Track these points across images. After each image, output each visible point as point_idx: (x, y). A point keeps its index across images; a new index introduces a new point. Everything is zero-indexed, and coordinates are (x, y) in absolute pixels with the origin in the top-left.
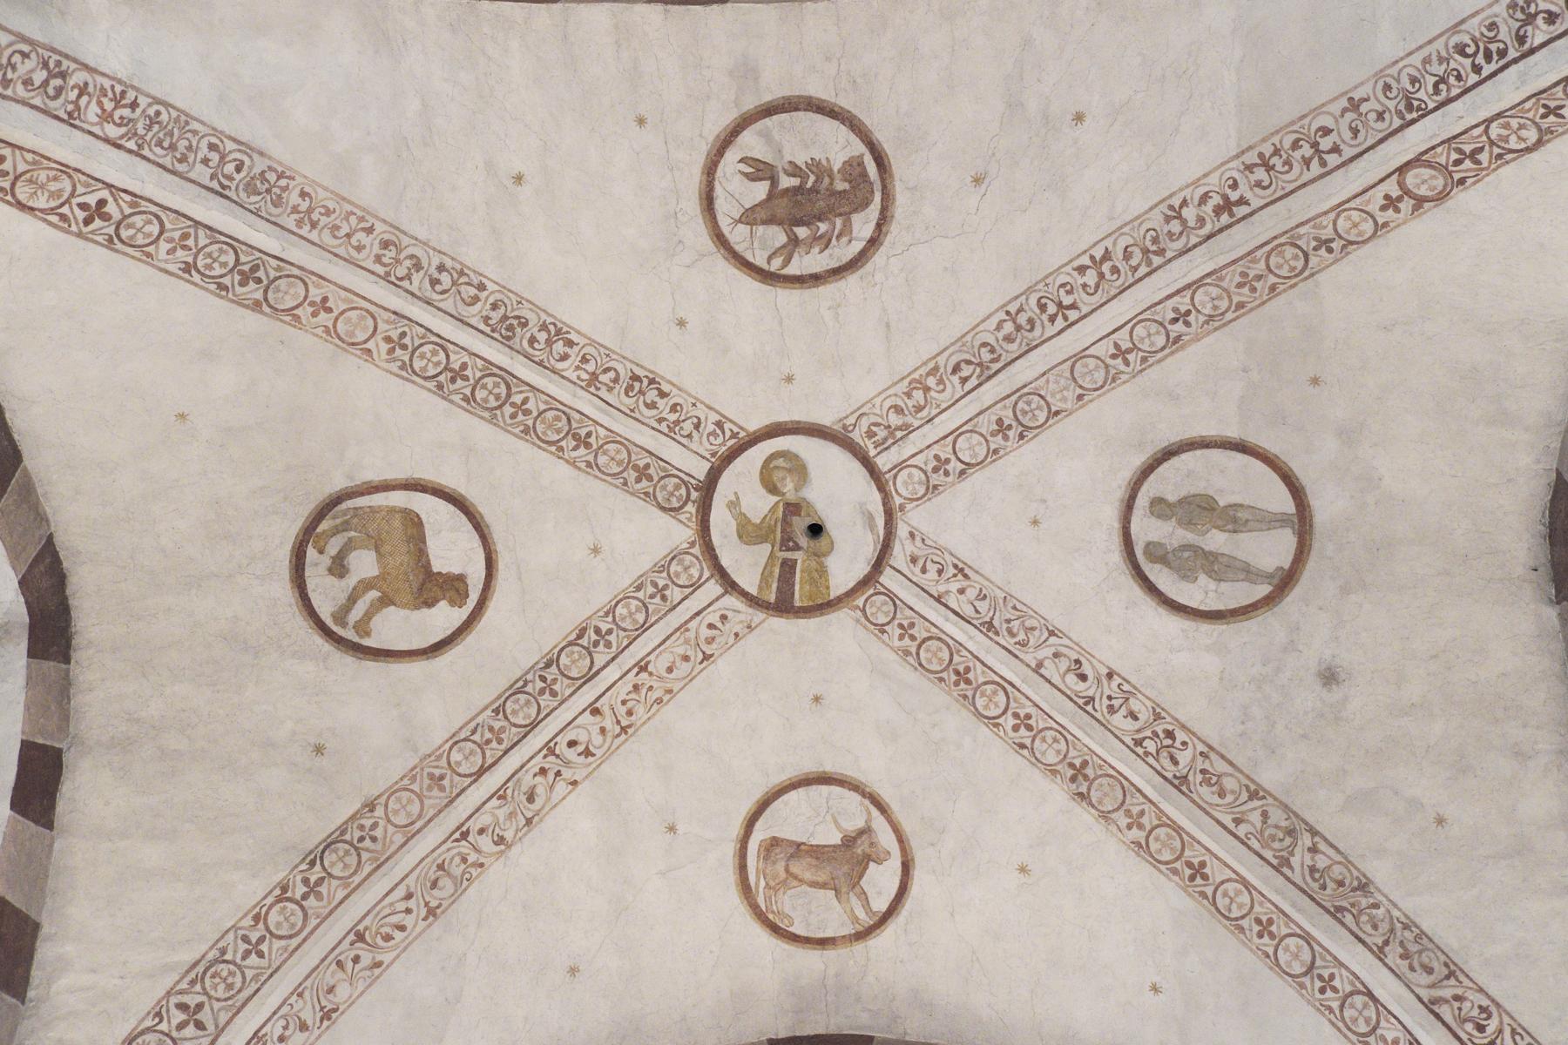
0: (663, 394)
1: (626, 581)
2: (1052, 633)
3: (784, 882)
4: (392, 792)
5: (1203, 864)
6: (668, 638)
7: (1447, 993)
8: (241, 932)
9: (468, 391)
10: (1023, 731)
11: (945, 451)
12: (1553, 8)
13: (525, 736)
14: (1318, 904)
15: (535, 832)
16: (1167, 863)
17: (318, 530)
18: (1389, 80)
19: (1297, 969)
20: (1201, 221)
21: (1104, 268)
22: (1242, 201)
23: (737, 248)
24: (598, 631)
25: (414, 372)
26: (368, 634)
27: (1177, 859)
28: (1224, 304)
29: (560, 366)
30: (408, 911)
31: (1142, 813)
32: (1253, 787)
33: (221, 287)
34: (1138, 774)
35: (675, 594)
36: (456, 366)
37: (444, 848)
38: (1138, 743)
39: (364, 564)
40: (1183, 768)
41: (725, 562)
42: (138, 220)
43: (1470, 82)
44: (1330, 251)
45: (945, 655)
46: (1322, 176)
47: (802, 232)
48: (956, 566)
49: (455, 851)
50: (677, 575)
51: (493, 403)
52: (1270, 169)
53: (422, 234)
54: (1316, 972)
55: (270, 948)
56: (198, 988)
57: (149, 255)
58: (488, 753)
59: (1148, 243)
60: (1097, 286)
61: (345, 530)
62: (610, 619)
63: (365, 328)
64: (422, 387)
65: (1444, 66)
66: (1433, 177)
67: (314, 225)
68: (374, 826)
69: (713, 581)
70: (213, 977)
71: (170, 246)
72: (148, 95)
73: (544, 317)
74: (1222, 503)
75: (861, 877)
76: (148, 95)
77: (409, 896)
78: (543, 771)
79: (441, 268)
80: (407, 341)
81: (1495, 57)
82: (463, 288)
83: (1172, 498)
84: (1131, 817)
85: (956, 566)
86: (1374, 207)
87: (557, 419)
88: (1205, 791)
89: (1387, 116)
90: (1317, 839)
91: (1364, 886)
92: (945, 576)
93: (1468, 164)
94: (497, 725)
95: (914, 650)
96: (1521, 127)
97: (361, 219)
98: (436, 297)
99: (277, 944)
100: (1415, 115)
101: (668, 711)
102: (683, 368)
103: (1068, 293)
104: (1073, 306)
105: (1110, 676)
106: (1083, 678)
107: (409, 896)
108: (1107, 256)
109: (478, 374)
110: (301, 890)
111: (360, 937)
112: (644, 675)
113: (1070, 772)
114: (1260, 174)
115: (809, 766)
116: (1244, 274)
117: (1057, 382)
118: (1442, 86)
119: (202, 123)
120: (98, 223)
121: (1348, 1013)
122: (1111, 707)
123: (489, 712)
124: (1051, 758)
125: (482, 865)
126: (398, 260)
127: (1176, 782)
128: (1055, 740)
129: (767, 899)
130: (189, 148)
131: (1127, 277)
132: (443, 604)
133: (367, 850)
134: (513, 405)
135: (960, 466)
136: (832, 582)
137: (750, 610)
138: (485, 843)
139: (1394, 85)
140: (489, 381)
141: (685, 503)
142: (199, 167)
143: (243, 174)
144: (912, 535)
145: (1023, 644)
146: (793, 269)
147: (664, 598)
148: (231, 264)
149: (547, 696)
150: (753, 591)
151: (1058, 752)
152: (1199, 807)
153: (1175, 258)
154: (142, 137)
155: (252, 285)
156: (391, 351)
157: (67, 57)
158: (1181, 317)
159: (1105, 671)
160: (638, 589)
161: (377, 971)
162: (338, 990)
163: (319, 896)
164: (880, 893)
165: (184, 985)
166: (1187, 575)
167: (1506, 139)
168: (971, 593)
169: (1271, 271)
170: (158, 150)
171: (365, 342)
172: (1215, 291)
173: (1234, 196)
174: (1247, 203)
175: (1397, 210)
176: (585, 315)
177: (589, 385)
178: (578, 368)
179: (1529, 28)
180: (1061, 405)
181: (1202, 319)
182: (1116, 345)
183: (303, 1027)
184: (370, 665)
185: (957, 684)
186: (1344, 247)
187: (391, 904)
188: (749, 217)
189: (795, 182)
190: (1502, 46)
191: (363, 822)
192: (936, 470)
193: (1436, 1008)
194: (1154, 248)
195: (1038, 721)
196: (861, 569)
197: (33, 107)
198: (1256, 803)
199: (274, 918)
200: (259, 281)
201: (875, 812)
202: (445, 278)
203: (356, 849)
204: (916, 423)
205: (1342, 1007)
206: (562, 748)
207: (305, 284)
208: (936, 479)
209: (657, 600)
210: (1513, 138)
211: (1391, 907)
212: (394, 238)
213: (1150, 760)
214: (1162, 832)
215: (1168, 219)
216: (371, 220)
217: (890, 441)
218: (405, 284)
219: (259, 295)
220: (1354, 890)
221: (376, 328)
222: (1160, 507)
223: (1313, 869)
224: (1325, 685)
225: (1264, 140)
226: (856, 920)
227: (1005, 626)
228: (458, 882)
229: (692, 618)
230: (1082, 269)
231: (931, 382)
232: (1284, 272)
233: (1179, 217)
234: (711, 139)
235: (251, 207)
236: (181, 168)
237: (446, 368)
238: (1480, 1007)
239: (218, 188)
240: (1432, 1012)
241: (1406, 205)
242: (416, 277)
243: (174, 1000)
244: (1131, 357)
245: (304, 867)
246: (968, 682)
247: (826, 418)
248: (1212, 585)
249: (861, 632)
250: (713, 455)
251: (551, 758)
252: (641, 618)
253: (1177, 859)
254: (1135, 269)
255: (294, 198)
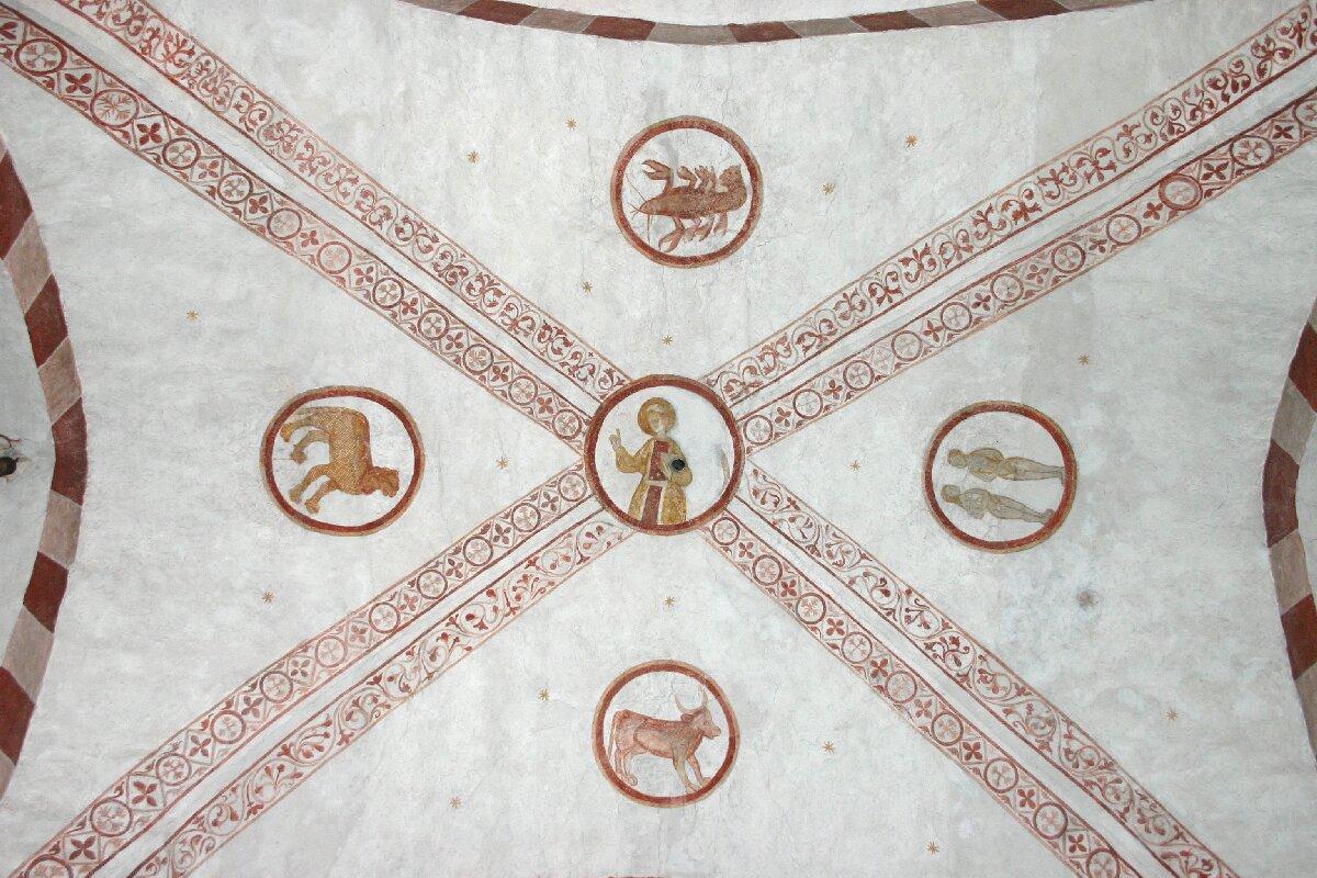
0: (567, 344)
1: (524, 491)
2: (863, 557)
3: (632, 747)
4: (322, 638)
5: (977, 746)
6: (553, 541)
7: (1176, 850)
8: (191, 734)
9: (415, 322)
10: (835, 635)
11: (786, 406)
12: (1287, 46)
13: (433, 606)
14: (1073, 779)
15: (434, 685)
16: (947, 744)
17: (287, 422)
18: (1156, 110)
19: (1052, 831)
20: (1003, 224)
21: (922, 260)
22: (1035, 208)
23: (636, 231)
24: (498, 529)
26: (316, 511)
27: (957, 741)
28: (1017, 292)
29: (489, 310)
30: (326, 735)
31: (930, 703)
32: (1021, 685)
33: (237, 211)
34: (928, 670)
35: (563, 505)
36: (409, 301)
37: (358, 689)
38: (929, 647)
39: (319, 454)
40: (964, 669)
41: (604, 484)
42: (181, 145)
43: (1220, 109)
44: (1102, 250)
45: (776, 571)
46: (1100, 188)
47: (688, 223)
48: (789, 500)
49: (369, 692)
50: (566, 490)
51: (434, 334)
52: (1058, 181)
53: (394, 190)
54: (1068, 834)
55: (213, 749)
56: (153, 772)
57: (185, 176)
58: (402, 616)
59: (960, 241)
60: (917, 275)
61: (308, 425)
62: (509, 520)
63: (342, 260)
64: (381, 315)
65: (1200, 98)
66: (1187, 189)
68: (306, 664)
69: (593, 498)
70: (166, 765)
71: (201, 171)
72: (203, 48)
73: (481, 269)
74: (1006, 457)
75: (696, 748)
76: (203, 48)
77: (328, 724)
78: (445, 636)
79: (406, 220)
80: (373, 274)
81: (1241, 87)
82: (421, 238)
83: (965, 450)
84: (920, 706)
85: (789, 500)
86: (1139, 215)
87: (483, 353)
88: (982, 687)
89: (1153, 138)
90: (1072, 728)
91: (1109, 765)
92: (781, 506)
93: (1214, 178)
94: (411, 595)
95: (751, 565)
96: (1258, 145)
97: (349, 171)
98: (399, 242)
99: (219, 747)
100: (1175, 137)
101: (550, 600)
102: (586, 323)
103: (894, 280)
104: (897, 291)
105: (909, 592)
106: (887, 593)
107: (328, 724)
108: (926, 251)
110: (242, 706)
111: (286, 751)
112: (532, 568)
113: (872, 669)
114: (1051, 186)
115: (659, 655)
116: (1034, 268)
117: (880, 353)
118: (1198, 113)
119: (240, 77)
120: (151, 143)
121: (1093, 868)
122: (908, 617)
123: (405, 584)
124: (857, 657)
125: (389, 707)
126: (377, 209)
127: (959, 679)
128: (862, 642)
129: (618, 761)
130: (227, 94)
131: (940, 268)
132: (378, 493)
133: (299, 682)
134: (449, 338)
135: (798, 418)
136: (688, 507)
137: (622, 525)
138: (393, 688)
139: (1160, 113)
140: (433, 316)
141: (577, 434)
142: (233, 111)
143: (264, 122)
144: (755, 472)
145: (840, 565)
146: (679, 252)
147: (553, 507)
148: (246, 193)
149: (453, 576)
150: (625, 510)
151: (863, 652)
152: (977, 699)
153: (980, 253)
154: (193, 79)
155: (259, 213)
157: (148, 6)
158: (983, 302)
159: (905, 588)
160: (534, 498)
161: (297, 781)
162: (264, 791)
163: (256, 714)
164: (709, 763)
165: (142, 769)
166: (976, 513)
167: (1244, 157)
168: (800, 522)
169: (1055, 266)
170: (203, 91)
171: (340, 272)
172: (1010, 281)
173: (1029, 204)
174: (1039, 209)
175: (1157, 217)
176: (514, 272)
177: (510, 329)
178: (503, 314)
179: (1269, 63)
180: (883, 372)
181: (998, 303)
182: (930, 325)
183: (234, 817)
184: (316, 535)
185: (784, 594)
186: (1114, 247)
187: (313, 728)
188: (648, 208)
189: (686, 183)
190: (1246, 79)
191: (297, 659)
192: (778, 420)
193: (1166, 861)
194: (964, 245)
195: (848, 627)
196: (713, 498)
197: (117, 37)
198: (1023, 698)
199: (219, 725)
200: (265, 210)
201: (711, 696)
203: (290, 680)
204: (766, 382)
205: (1088, 864)
206: (461, 619)
207: (300, 218)
208: (777, 428)
209: (548, 509)
210: (1251, 156)
211: (1130, 782)
212: (372, 190)
213: (939, 661)
214: (945, 718)
215: (976, 222)
216: (357, 173)
217: (744, 395)
218: (377, 228)
219: (264, 222)
220: (1101, 768)
222: (955, 456)
223: (1068, 752)
224: (1082, 606)
225: (1056, 160)
226: (688, 784)
227: (826, 549)
228: (368, 718)
229: (575, 527)
230: (906, 261)
231: (780, 349)
232: (1065, 267)
233: (985, 220)
234: (624, 142)
235: (268, 149)
236: (218, 108)
237: (400, 301)
238: (1203, 861)
239: (244, 129)
240: (1164, 864)
241: (1165, 212)
242: (386, 224)
243: (134, 779)
244: (940, 334)
245: (246, 688)
246: (793, 593)
247: (694, 374)
248: (995, 521)
249: (709, 550)
250: (602, 397)
251: (452, 627)
252: (534, 521)
253: (957, 741)
254: (948, 261)
255: (300, 148)
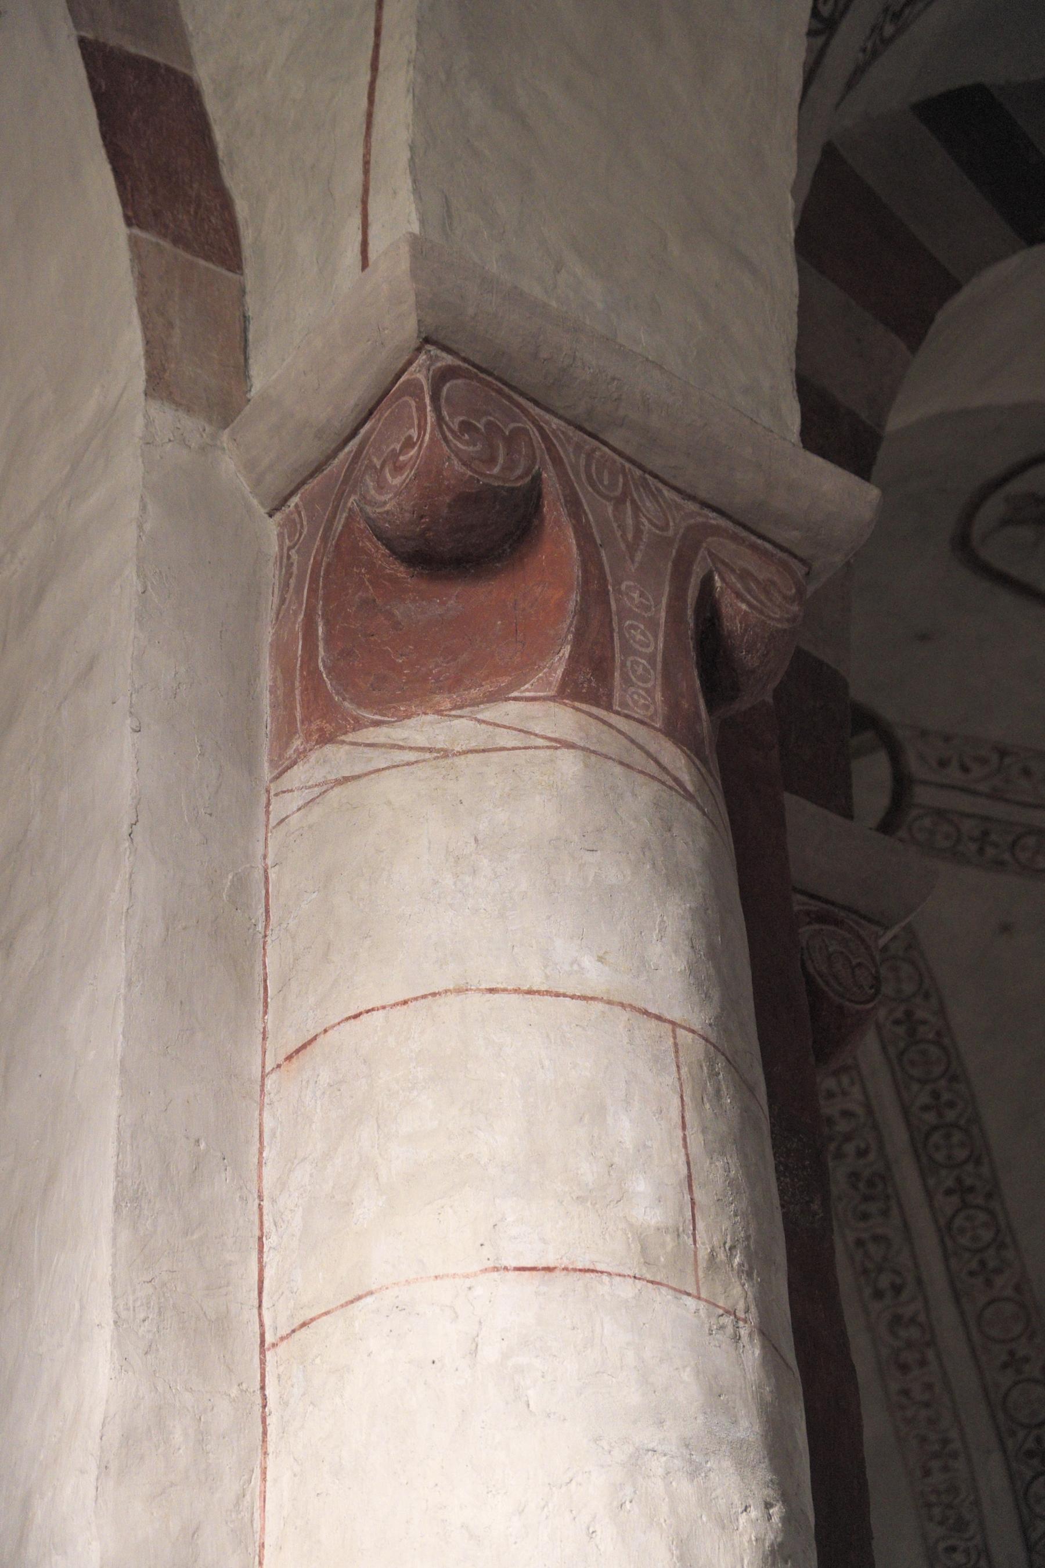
9: (970, 1167)
25: (998, 1232)
36: (955, 1199)
51: (957, 1137)
67: (945, 1442)
79: (878, 1295)
109: (944, 1172)
134: (940, 1115)
140: (940, 1157)
156: (998, 1271)
178: (844, 1093)
202: (884, 1281)
221: (989, 1303)
